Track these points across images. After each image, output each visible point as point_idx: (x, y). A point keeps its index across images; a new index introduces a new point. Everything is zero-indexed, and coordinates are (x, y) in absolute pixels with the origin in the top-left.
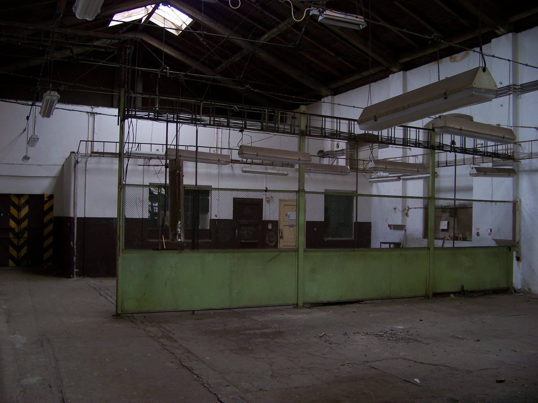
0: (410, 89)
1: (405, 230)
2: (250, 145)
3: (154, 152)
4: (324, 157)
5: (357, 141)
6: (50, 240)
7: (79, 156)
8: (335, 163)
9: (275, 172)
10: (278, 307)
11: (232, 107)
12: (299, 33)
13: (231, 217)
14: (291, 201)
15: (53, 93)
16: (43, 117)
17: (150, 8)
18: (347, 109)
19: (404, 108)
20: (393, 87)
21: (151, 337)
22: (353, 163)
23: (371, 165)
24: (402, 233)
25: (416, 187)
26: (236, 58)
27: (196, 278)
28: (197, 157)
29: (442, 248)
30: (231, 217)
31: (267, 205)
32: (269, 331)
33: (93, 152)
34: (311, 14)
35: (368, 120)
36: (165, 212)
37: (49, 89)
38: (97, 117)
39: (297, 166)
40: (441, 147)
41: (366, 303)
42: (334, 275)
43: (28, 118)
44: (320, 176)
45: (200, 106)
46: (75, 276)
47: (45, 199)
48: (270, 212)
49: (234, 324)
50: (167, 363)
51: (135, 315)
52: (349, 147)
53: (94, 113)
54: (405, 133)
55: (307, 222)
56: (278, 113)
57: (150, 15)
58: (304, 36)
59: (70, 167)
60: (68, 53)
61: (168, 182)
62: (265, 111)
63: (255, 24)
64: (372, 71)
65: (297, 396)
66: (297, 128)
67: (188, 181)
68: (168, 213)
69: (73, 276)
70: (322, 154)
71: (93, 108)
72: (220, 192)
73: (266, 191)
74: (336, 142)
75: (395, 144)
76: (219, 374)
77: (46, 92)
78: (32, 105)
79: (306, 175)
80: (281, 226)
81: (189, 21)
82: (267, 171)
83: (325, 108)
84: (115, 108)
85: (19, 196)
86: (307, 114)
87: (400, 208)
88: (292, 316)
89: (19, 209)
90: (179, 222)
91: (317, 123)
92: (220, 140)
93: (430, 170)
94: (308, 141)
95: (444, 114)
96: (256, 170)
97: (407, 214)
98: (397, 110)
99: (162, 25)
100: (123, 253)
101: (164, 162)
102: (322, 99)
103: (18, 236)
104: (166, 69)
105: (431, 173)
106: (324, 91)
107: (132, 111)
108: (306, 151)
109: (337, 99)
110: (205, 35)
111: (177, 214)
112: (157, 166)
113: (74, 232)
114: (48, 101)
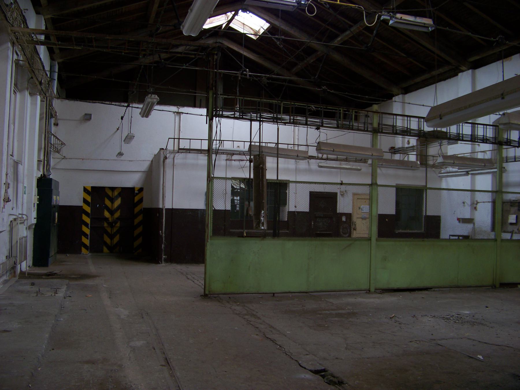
0: (479, 87)
1: (474, 223)
2: (325, 141)
3: (235, 148)
4: (395, 154)
5: (426, 138)
6: (140, 230)
7: (168, 152)
8: (406, 159)
9: (349, 167)
10: (351, 292)
11: (310, 107)
12: (370, 35)
13: (307, 210)
14: (365, 194)
15: (153, 96)
16: (143, 117)
17: (230, 15)
18: (415, 107)
19: (466, 108)
20: (461, 86)
21: (236, 314)
22: (423, 158)
23: (440, 160)
24: (470, 226)
25: (484, 182)
26: (311, 60)
27: (276, 263)
28: (278, 152)
29: (511, 240)
30: (307, 210)
31: (341, 198)
32: (343, 312)
33: (179, 149)
34: (382, 18)
35: (434, 118)
36: (249, 203)
37: (150, 93)
38: (182, 116)
39: (370, 162)
40: (509, 143)
41: (434, 291)
42: (404, 263)
43: (122, 118)
44: (391, 171)
45: (281, 106)
46: (163, 262)
47: (136, 192)
48: (344, 205)
49: (311, 305)
50: (252, 335)
51: (221, 295)
52: (419, 143)
53: (180, 113)
54: (473, 130)
55: (379, 215)
56: (352, 112)
57: (230, 22)
58: (375, 38)
59: (159, 162)
60: (156, 58)
61: (252, 177)
62: (340, 110)
63: (329, 28)
64: (441, 70)
65: (369, 365)
66: (370, 126)
67: (270, 176)
68: (252, 204)
69: (161, 262)
70: (394, 150)
71: (179, 108)
72: (298, 185)
73: (342, 184)
74: (407, 138)
75: (463, 140)
76: (299, 345)
77: (147, 95)
78: (128, 106)
79: (379, 171)
80: (354, 219)
81: (266, 25)
82: (342, 166)
83: (396, 107)
84: (203, 107)
85: (113, 189)
86: (379, 113)
87: (468, 201)
88: (364, 300)
89: (112, 200)
90: (263, 212)
91: (388, 121)
92: (297, 137)
93: (497, 165)
94: (380, 138)
95: (509, 111)
96: (331, 166)
97: (475, 208)
98: (460, 110)
99: (242, 31)
100: (211, 240)
101: (248, 157)
102: (394, 98)
103: (111, 225)
104: (246, 71)
105: (498, 168)
106: (395, 90)
107: (219, 111)
108: (378, 147)
109: (410, 97)
110: (283, 39)
111: (259, 206)
112: (242, 160)
113: (162, 222)
114: (149, 103)
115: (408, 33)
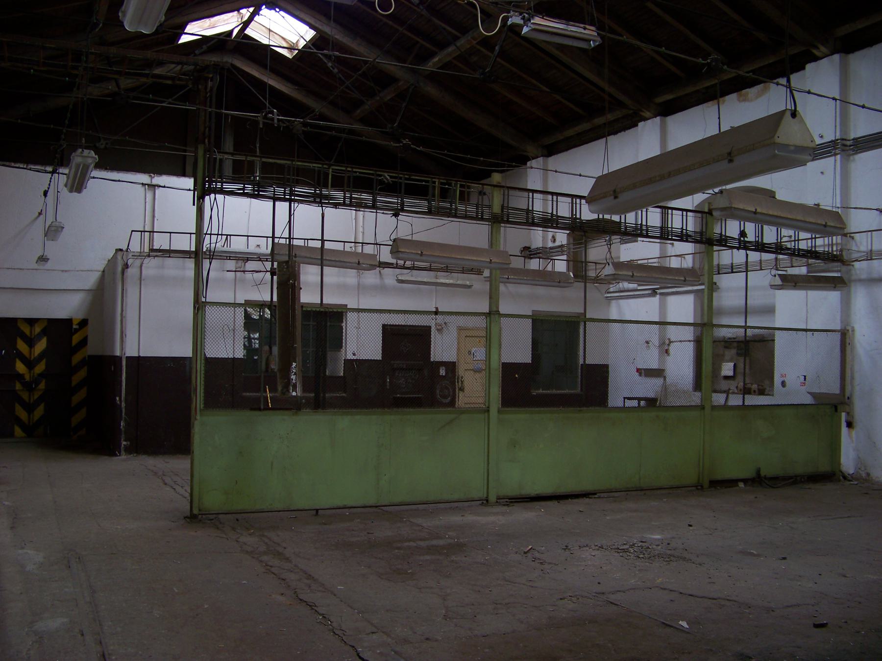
0: (672, 146)
1: (665, 377)
2: (409, 238)
3: (252, 249)
4: (531, 258)
5: (585, 232)
6: (82, 394)
7: (130, 256)
8: (549, 268)
9: (451, 281)
10: (456, 504)
11: (381, 176)
12: (490, 54)
13: (378, 356)
14: (478, 329)
15: (86, 152)
16: (71, 191)
17: (246, 13)
18: (568, 178)
19: (662, 178)
20: (644, 143)
21: (247, 552)
22: (579, 267)
23: (609, 270)
24: (658, 381)
25: (682, 307)
26: (387, 95)
27: (321, 457)
28: (323, 257)
29: (725, 407)
30: (378, 356)
31: (438, 336)
32: (441, 542)
33: (152, 250)
34: (509, 23)
35: (604, 196)
36: (271, 348)
37: (81, 147)
38: (158, 191)
39: (487, 273)
40: (723, 241)
41: (599, 497)
42: (547, 451)
43: (45, 194)
44: (524, 289)
45: (328, 174)
46: (123, 452)
47: (74, 327)
48: (443, 348)
49: (384, 531)
50: (273, 596)
51: (221, 516)
52: (571, 241)
53: (154, 186)
54: (664, 219)
55: (503, 364)
56: (456, 185)
57: (246, 24)
58: (498, 59)
59: (114, 273)
60: (111, 87)
61: (275, 299)
62: (434, 182)
63: (418, 39)
64: (610, 117)
65: (487, 650)
66: (486, 210)
67: (308, 297)
68: (275, 350)
69: (120, 452)
70: (528, 253)
71: (152, 178)
72: (361, 314)
73: (436, 313)
74: (551, 232)
75: (647, 236)
76: (359, 613)
77: (75, 151)
78: (53, 172)
79: (502, 288)
80: (461, 371)
81: (309, 34)
82: (438, 281)
83: (533, 177)
84: (189, 176)
85: (31, 322)
86: (503, 187)
87: (655, 341)
88: (479, 518)
89: (31, 342)
90: (294, 365)
91: (519, 202)
92: (361, 229)
93: (705, 279)
94: (505, 231)
95: (729, 187)
96: (419, 279)
97: (667, 351)
98: (650, 181)
99: (265, 41)
100: (201, 415)
101: (268, 265)
102: (528, 163)
103: (29, 387)
104: (272, 113)
105: (706, 284)
106: (530, 149)
107: (216, 182)
108: (502, 248)
109: (553, 162)
110: (336, 57)
111: (291, 352)
112: (257, 272)
113: (121, 381)
114: (78, 166)
115: (556, 52)
